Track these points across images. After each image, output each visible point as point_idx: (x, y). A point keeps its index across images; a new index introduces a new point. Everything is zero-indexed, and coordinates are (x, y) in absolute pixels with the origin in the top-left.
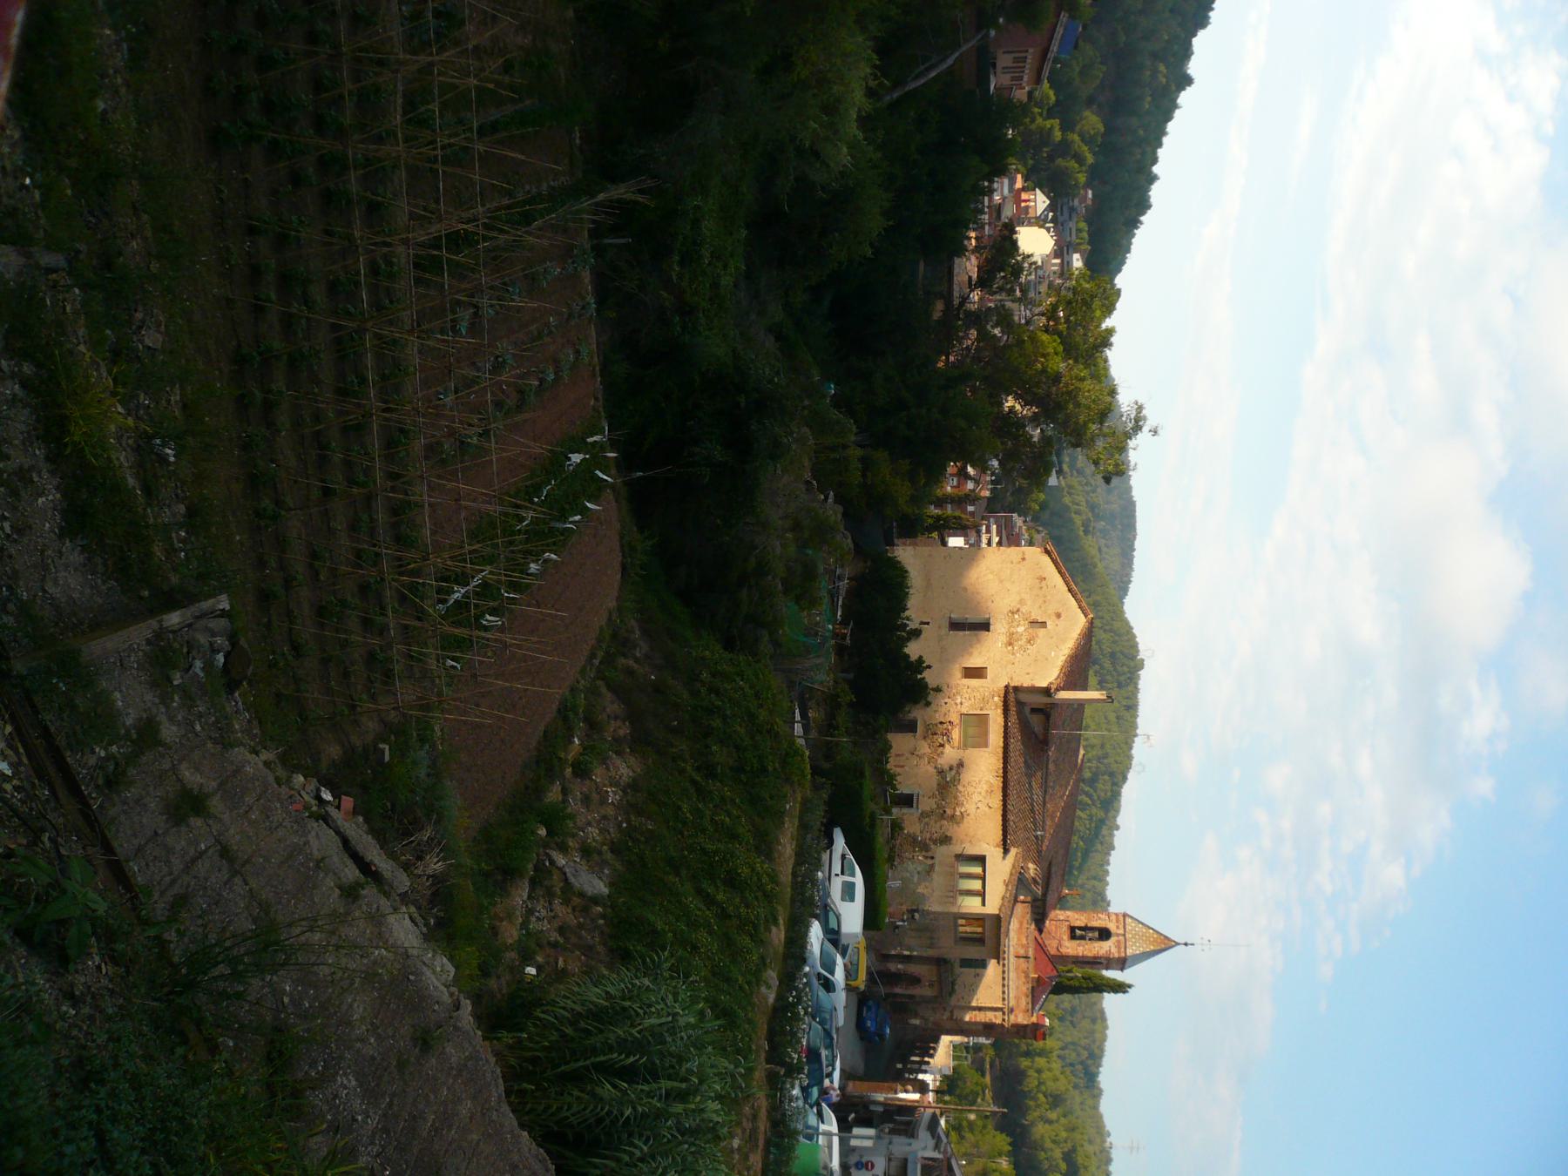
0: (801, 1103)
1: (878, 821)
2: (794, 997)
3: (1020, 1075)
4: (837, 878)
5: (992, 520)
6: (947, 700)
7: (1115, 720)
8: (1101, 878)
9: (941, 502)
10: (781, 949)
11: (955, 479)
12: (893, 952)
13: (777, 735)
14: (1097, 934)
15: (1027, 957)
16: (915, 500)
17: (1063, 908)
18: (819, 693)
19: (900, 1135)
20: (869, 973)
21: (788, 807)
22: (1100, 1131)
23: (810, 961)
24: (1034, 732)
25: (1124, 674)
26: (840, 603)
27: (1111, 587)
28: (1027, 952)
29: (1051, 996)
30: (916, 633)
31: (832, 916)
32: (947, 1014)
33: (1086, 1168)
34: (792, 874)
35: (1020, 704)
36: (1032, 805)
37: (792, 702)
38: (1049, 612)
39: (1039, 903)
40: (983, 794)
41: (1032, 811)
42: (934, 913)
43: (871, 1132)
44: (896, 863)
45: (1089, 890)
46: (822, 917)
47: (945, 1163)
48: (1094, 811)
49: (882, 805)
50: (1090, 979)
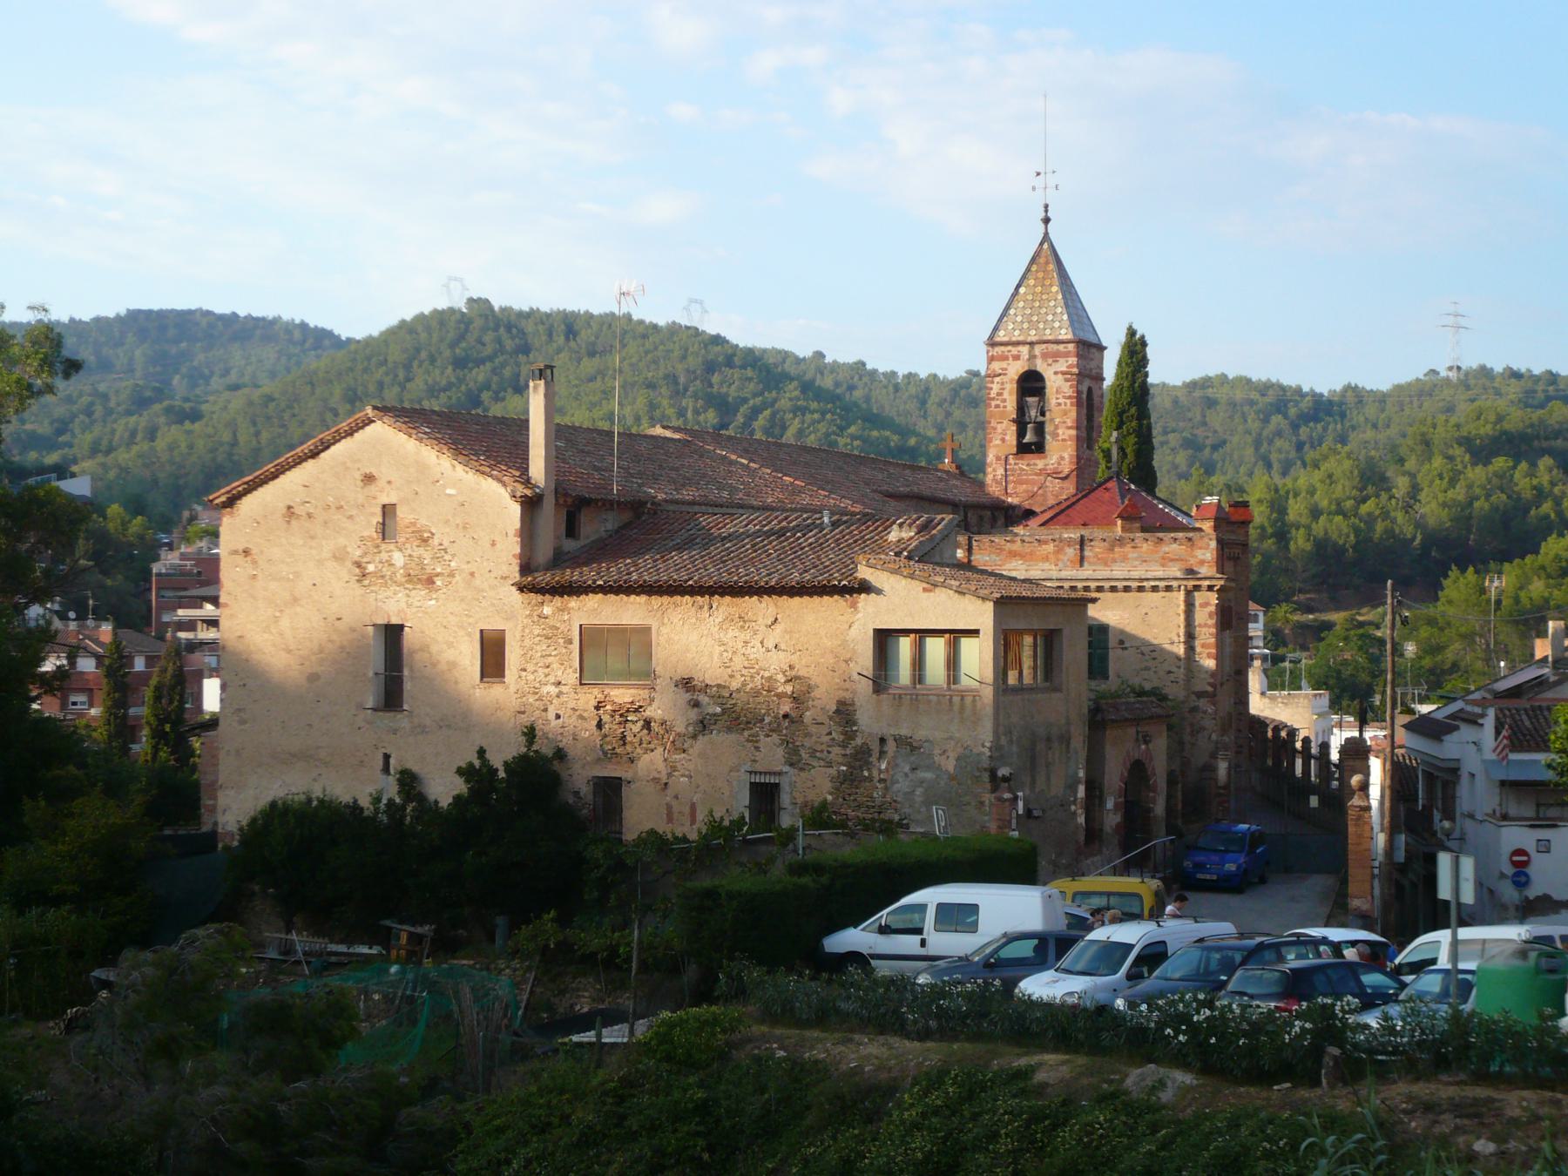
0: (1394, 1010)
1: (810, 857)
2: (1177, 1032)
3: (1324, 550)
5: (166, 618)
6: (551, 715)
7: (596, 360)
8: (923, 390)
9: (123, 730)
10: (1081, 1060)
11: (73, 699)
12: (1081, 820)
13: (627, 1082)
14: (1031, 400)
15: (1082, 542)
16: (115, 788)
17: (981, 467)
18: (538, 990)
19: (1453, 797)
20: (1125, 869)
21: (782, 1053)
22: (1425, 389)
23: (1102, 997)
24: (617, 532)
25: (499, 341)
26: (342, 948)
27: (313, 366)
28: (1070, 542)
29: (1161, 491)
30: (409, 781)
31: (1010, 952)
33: (1500, 419)
34: (920, 1039)
35: (559, 560)
36: (768, 534)
37: (556, 1051)
38: (361, 499)
39: (973, 518)
40: (747, 635)
41: (781, 533)
42: (996, 733)
43: (1444, 860)
44: (897, 818)
45: (948, 414)
46: (1009, 973)
47: (1505, 703)
49: (774, 849)
50: (1120, 415)
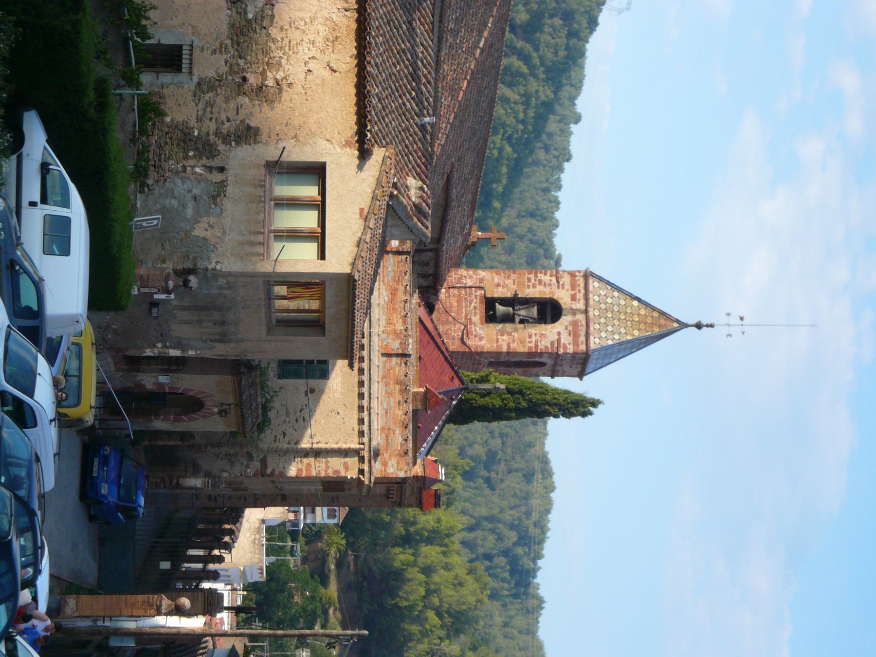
4: (34, 210)
12: (148, 353)
14: (534, 311)
20: (103, 393)
28: (404, 344)
32: (256, 464)
36: (414, 64)
39: (428, 256)
41: (415, 77)
42: (230, 274)
44: (150, 182)
45: (521, 238)
48: (533, 85)
50: (520, 392)
